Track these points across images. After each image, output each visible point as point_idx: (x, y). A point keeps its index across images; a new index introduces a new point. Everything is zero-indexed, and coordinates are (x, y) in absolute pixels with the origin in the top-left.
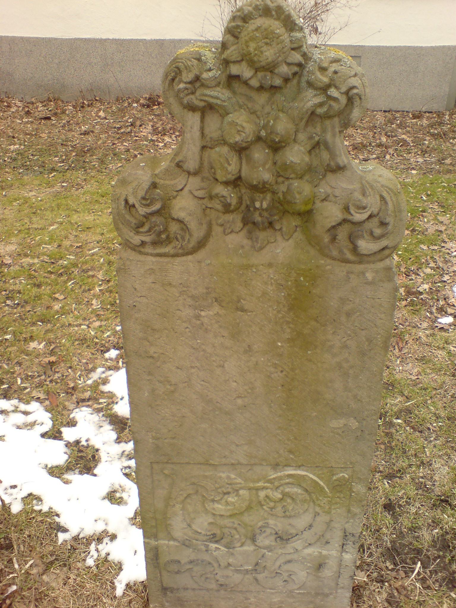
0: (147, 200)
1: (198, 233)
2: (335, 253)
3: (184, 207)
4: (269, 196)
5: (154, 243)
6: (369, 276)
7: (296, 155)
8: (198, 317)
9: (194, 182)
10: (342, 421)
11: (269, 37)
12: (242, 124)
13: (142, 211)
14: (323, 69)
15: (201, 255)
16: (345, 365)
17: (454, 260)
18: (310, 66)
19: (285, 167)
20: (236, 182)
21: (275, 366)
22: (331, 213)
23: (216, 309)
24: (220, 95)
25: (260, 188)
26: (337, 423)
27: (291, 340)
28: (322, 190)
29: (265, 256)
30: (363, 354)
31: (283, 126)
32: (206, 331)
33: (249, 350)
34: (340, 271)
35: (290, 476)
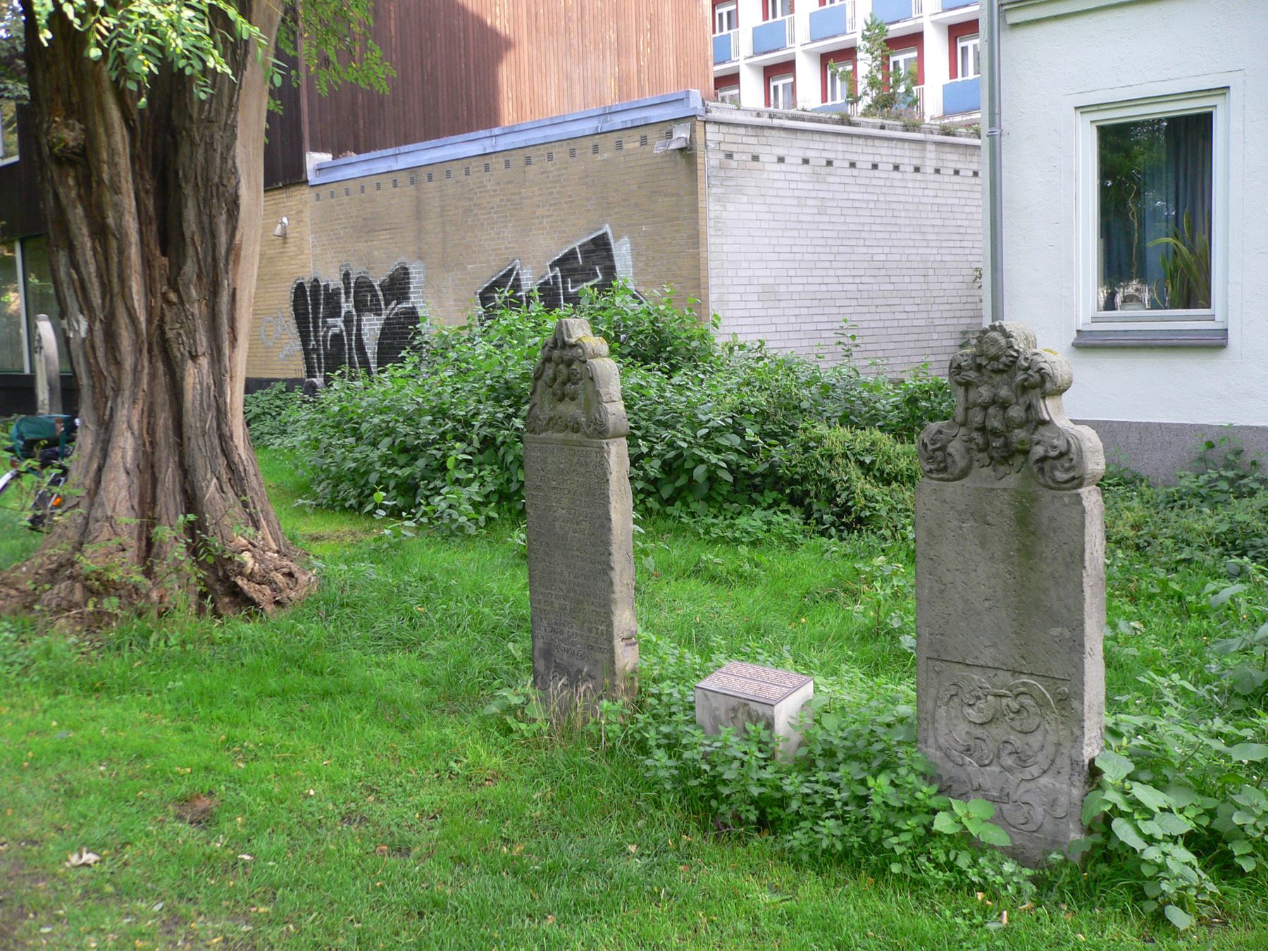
0: (934, 442)
1: (961, 463)
2: (1042, 480)
3: (955, 448)
4: (1002, 440)
5: (938, 471)
6: (1066, 500)
7: (1016, 412)
8: (961, 528)
9: (963, 430)
10: (1059, 630)
11: (995, 342)
12: (984, 393)
13: (930, 447)
14: (1026, 359)
15: (963, 481)
16: (1009, 761)
17: (860, 6)
18: (1021, 358)
19: (1010, 419)
20: (982, 429)
21: (1010, 573)
22: (1039, 451)
23: (972, 522)
24: (972, 375)
25: (995, 433)
26: (1055, 631)
27: (1018, 550)
28: (1036, 437)
29: (1002, 484)
30: (1067, 565)
31: (1004, 392)
32: (966, 539)
33: (992, 558)
34: (1047, 495)
35: (1024, 684)
